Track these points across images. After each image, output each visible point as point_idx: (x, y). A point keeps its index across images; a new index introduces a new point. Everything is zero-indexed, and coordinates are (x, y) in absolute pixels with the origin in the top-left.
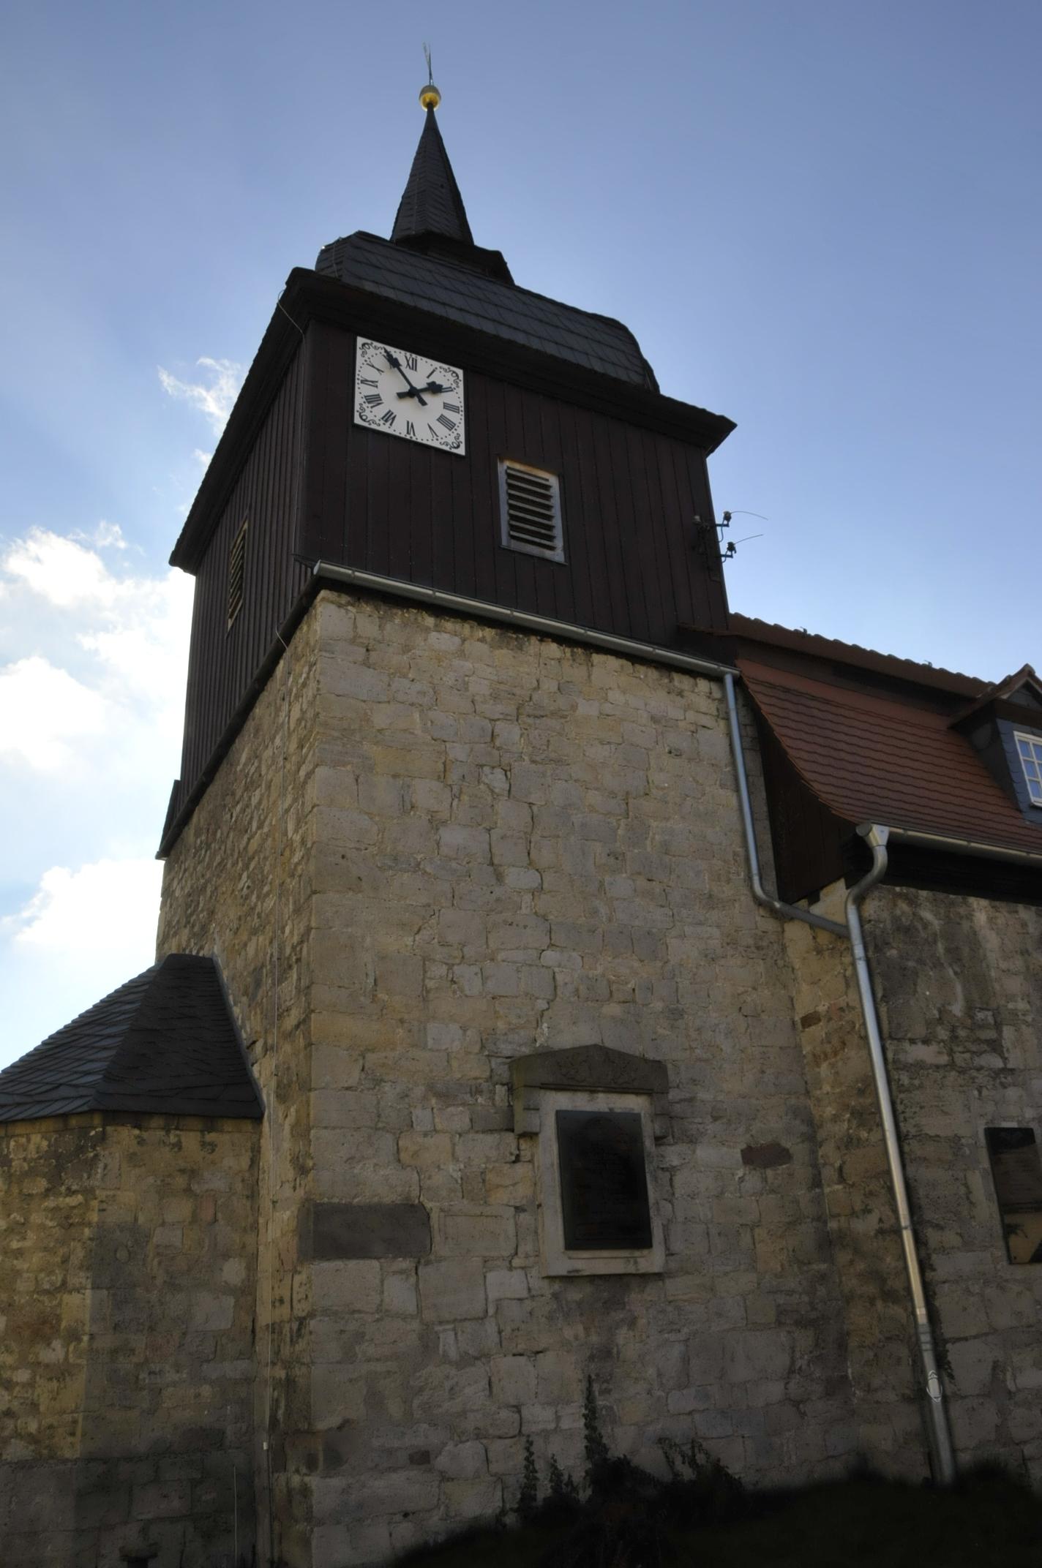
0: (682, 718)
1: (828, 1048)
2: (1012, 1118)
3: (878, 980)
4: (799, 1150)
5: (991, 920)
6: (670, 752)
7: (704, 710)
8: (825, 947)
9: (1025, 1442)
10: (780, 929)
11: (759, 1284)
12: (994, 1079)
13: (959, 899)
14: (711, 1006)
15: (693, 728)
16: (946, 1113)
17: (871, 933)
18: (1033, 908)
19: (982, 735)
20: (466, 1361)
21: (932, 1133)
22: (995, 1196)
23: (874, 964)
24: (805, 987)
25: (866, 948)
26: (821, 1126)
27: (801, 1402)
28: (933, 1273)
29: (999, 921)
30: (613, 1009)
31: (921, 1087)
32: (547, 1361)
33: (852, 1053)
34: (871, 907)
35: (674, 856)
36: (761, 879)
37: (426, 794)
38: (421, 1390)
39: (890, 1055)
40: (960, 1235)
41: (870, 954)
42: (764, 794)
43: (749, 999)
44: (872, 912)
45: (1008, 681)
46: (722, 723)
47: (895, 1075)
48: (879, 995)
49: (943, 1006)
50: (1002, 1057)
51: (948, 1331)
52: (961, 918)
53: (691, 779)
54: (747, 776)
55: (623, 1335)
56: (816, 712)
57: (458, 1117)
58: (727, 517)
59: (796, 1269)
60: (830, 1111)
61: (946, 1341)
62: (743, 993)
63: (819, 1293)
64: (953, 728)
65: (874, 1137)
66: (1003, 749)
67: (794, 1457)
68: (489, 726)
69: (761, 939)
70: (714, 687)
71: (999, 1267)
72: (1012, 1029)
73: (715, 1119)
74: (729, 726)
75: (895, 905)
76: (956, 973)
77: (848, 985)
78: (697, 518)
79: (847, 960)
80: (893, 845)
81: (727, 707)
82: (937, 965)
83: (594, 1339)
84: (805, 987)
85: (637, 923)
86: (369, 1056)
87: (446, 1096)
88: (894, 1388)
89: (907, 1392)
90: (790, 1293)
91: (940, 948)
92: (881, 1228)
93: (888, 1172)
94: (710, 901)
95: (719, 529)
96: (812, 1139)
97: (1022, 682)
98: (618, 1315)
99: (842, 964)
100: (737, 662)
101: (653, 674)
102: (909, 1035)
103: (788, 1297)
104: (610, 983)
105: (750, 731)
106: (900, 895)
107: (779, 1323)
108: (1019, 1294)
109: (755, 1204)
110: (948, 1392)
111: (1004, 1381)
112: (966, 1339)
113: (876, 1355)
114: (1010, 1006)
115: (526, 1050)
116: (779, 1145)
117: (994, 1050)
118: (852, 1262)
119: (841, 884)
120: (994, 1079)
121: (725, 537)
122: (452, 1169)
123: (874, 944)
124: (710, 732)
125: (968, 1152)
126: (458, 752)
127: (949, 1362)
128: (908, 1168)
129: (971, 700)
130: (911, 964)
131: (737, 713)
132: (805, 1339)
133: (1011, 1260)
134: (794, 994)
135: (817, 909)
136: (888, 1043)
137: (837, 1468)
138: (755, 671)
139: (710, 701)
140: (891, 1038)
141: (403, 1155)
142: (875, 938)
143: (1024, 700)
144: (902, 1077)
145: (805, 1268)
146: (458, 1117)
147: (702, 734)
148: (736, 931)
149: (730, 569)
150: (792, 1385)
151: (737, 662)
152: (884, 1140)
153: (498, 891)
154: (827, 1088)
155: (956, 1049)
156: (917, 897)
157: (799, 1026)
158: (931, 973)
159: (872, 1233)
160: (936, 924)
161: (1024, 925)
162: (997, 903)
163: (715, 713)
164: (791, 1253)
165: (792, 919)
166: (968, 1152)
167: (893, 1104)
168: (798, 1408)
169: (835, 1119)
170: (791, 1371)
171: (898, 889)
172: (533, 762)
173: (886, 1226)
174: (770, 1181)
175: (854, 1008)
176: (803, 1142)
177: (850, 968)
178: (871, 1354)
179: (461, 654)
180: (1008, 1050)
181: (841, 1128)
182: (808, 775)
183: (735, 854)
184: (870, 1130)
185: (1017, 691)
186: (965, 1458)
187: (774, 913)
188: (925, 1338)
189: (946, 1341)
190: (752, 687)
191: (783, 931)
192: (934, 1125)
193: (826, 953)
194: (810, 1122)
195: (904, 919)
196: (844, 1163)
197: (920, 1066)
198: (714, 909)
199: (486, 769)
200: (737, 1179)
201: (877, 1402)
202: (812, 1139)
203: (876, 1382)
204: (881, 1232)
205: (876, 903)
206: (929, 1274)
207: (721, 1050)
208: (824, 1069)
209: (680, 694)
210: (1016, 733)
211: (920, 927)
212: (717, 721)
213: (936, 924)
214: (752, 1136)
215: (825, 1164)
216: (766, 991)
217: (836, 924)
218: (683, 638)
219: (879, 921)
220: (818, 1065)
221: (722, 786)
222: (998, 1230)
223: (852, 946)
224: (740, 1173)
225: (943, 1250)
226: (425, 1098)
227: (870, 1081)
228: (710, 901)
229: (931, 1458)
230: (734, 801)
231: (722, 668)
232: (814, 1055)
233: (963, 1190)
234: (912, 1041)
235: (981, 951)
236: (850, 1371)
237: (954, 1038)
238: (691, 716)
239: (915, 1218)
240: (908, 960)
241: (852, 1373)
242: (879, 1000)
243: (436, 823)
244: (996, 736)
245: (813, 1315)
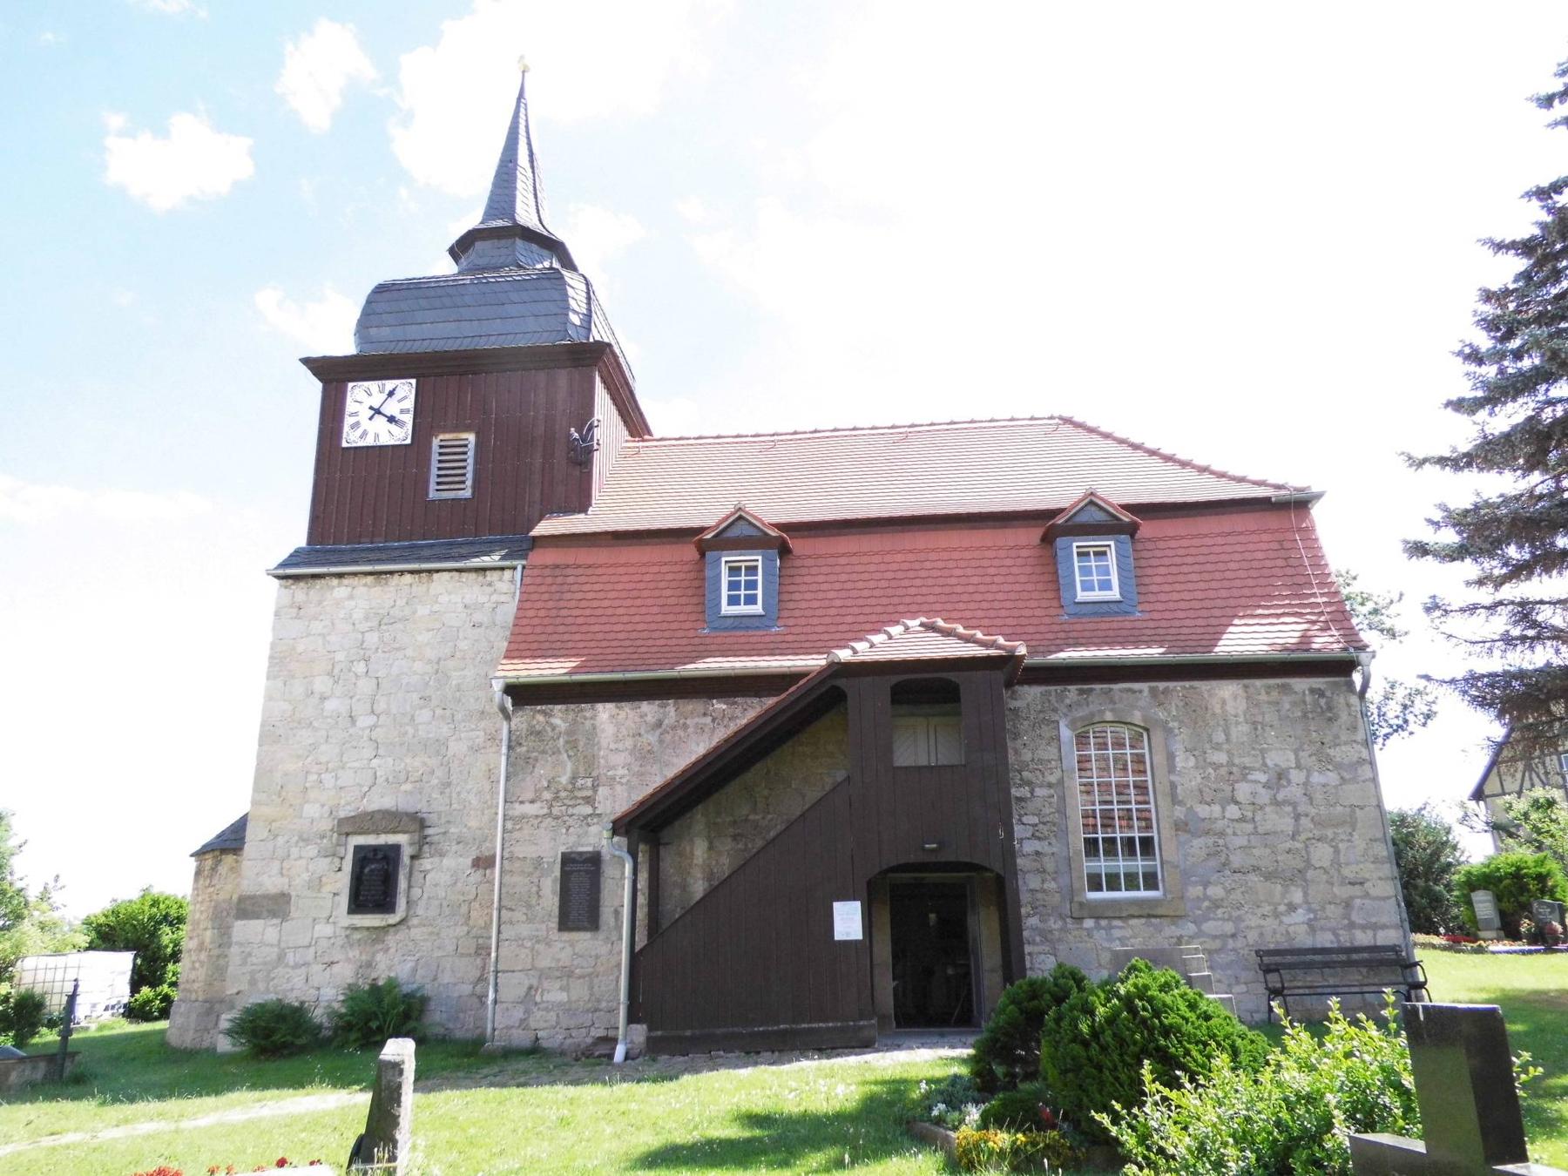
18: (657, 702)
20: (296, 966)
30: (408, 787)
32: (336, 968)
37: (321, 684)
38: (274, 978)
55: (379, 957)
57: (312, 850)
68: (360, 636)
73: (458, 843)
76: (569, 757)
83: (364, 958)
85: (431, 736)
86: (274, 824)
87: (304, 839)
98: (380, 947)
101: (473, 576)
104: (408, 772)
112: (513, 971)
115: (353, 814)
117: (588, 803)
122: (305, 876)
126: (340, 656)
141: (284, 871)
146: (312, 850)
153: (351, 731)
172: (384, 652)
179: (351, 597)
199: (355, 663)
209: (490, 585)
226: (297, 842)
233: (535, 889)
237: (556, 798)
243: (323, 699)
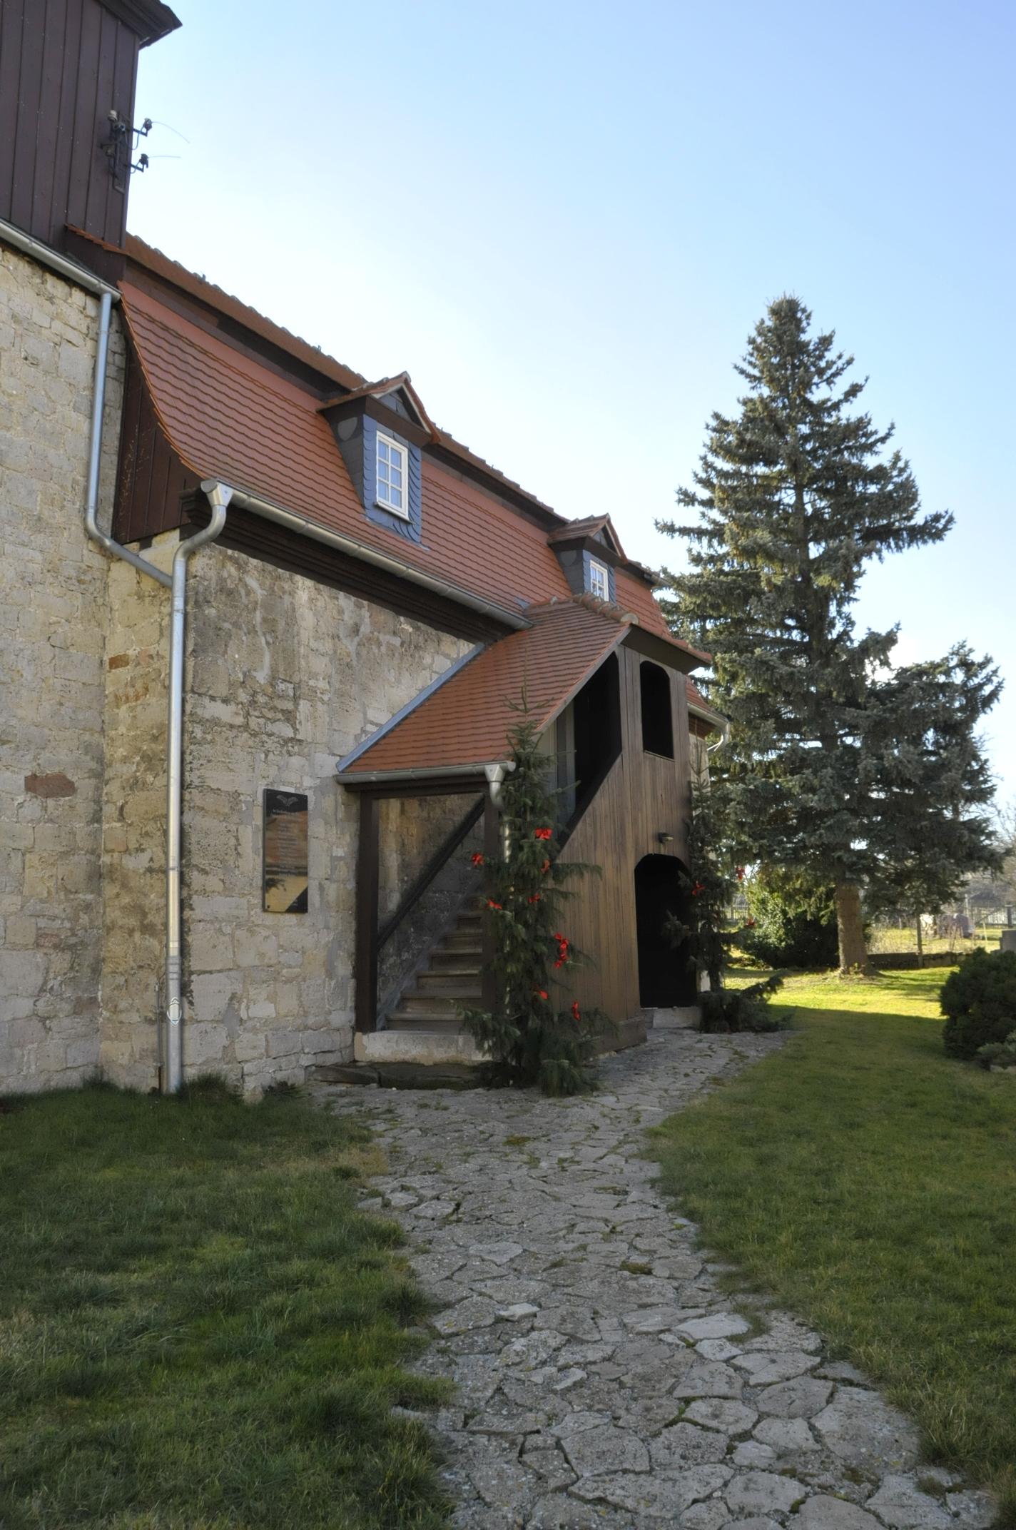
0: (48, 326)
1: (131, 692)
2: (290, 784)
3: (192, 635)
4: (85, 785)
5: (311, 600)
6: (26, 359)
7: (73, 323)
8: (147, 594)
9: (247, 1061)
10: (106, 568)
11: (22, 907)
12: (282, 746)
13: (287, 574)
14: (18, 631)
15: (57, 340)
16: (231, 770)
17: (194, 588)
18: (353, 599)
19: (347, 427)
21: (214, 786)
22: (261, 851)
23: (191, 619)
24: (119, 628)
25: (186, 603)
26: (110, 765)
27: (48, 1018)
28: (191, 912)
29: (319, 604)
31: (212, 742)
33: (151, 699)
34: (199, 563)
35: (8, 469)
36: (96, 512)
39: (188, 708)
40: (223, 881)
41: (189, 608)
42: (118, 429)
43: (60, 630)
44: (199, 568)
45: (383, 384)
46: (90, 343)
47: (189, 727)
48: (190, 649)
49: (249, 671)
50: (293, 728)
51: (195, 964)
52: (284, 593)
53: (43, 393)
54: (104, 405)
56: (191, 360)
58: (148, 125)
59: (62, 897)
60: (122, 752)
61: (191, 973)
62: (54, 623)
63: (81, 921)
64: (322, 413)
65: (159, 782)
66: (362, 445)
67: (33, 1067)
69: (85, 573)
70: (90, 302)
71: (252, 913)
72: (309, 704)
74: (96, 348)
75: (223, 566)
76: (268, 643)
77: (161, 635)
78: (114, 114)
79: (166, 610)
80: (234, 509)
81: (99, 328)
82: (252, 631)
84: (119, 628)
88: (138, 1010)
89: (150, 1015)
90: (53, 918)
91: (258, 616)
92: (150, 867)
93: (166, 816)
94: (38, 523)
95: (135, 135)
96: (99, 776)
97: (396, 387)
99: (160, 613)
100: (120, 283)
101: (24, 268)
102: (210, 692)
103: (50, 922)
105: (119, 360)
106: (231, 558)
107: (38, 945)
108: (266, 937)
109: (31, 831)
110: (186, 1017)
111: (239, 1010)
112: (211, 972)
113: (126, 981)
114: (311, 683)
116: (64, 777)
117: (288, 720)
118: (118, 895)
119: (176, 534)
120: (282, 746)
121: (140, 146)
123: (195, 599)
124: (75, 348)
125: (244, 808)
127: (191, 991)
128: (185, 815)
129: (346, 391)
130: (227, 625)
131: (108, 337)
132: (60, 961)
133: (265, 909)
134: (108, 634)
135: (147, 555)
136: (189, 696)
137: (74, 1079)
138: (136, 298)
139: (82, 316)
140: (193, 692)
142: (197, 594)
143: (393, 404)
144: (196, 730)
145: (72, 897)
147: (65, 349)
148: (60, 560)
149: (138, 183)
150: (41, 1004)
151: (120, 283)
152: (167, 786)
154: (122, 729)
155: (252, 712)
156: (246, 564)
157: (107, 666)
158: (244, 638)
159: (141, 871)
160: (260, 594)
161: (341, 612)
162: (321, 586)
163: (85, 331)
164: (60, 881)
165: (120, 560)
166: (244, 808)
167: (183, 753)
168: (44, 1024)
169: (125, 760)
170: (42, 990)
171: (230, 552)
173: (156, 865)
174: (50, 809)
175: (163, 657)
176: (89, 778)
177: (167, 618)
178: (121, 980)
180: (300, 722)
181: (129, 770)
182: (165, 419)
183: (75, 481)
184: (156, 775)
185: (390, 394)
186: (192, 1073)
187: (103, 549)
188: (174, 969)
189: (191, 973)
190: (130, 314)
191: (109, 570)
192: (217, 778)
193: (147, 600)
194: (100, 760)
195: (229, 581)
196: (127, 803)
197: (215, 722)
198: (40, 532)
200: (16, 803)
201: (121, 1022)
202: (99, 776)
203: (123, 1005)
204: (150, 870)
205: (206, 560)
206: (187, 913)
207: (22, 675)
208: (123, 711)
209: (51, 299)
210: (378, 433)
211: (243, 592)
212: (84, 340)
213: (260, 594)
214: (39, 765)
215: (107, 802)
216: (80, 626)
217: (162, 573)
218: (67, 241)
219: (204, 578)
220: (118, 707)
221: (76, 409)
222: (259, 882)
223: (173, 597)
224: (20, 799)
225: (204, 892)
227: (165, 729)
228: (38, 523)
229: (161, 1072)
230: (85, 427)
231: (102, 285)
232: (116, 696)
234: (213, 698)
235: (296, 628)
236: (100, 993)
237: (253, 702)
238: (57, 325)
239: (184, 861)
240: (224, 621)
241: (102, 995)
242: (188, 653)
244: (360, 430)
245: (73, 940)
